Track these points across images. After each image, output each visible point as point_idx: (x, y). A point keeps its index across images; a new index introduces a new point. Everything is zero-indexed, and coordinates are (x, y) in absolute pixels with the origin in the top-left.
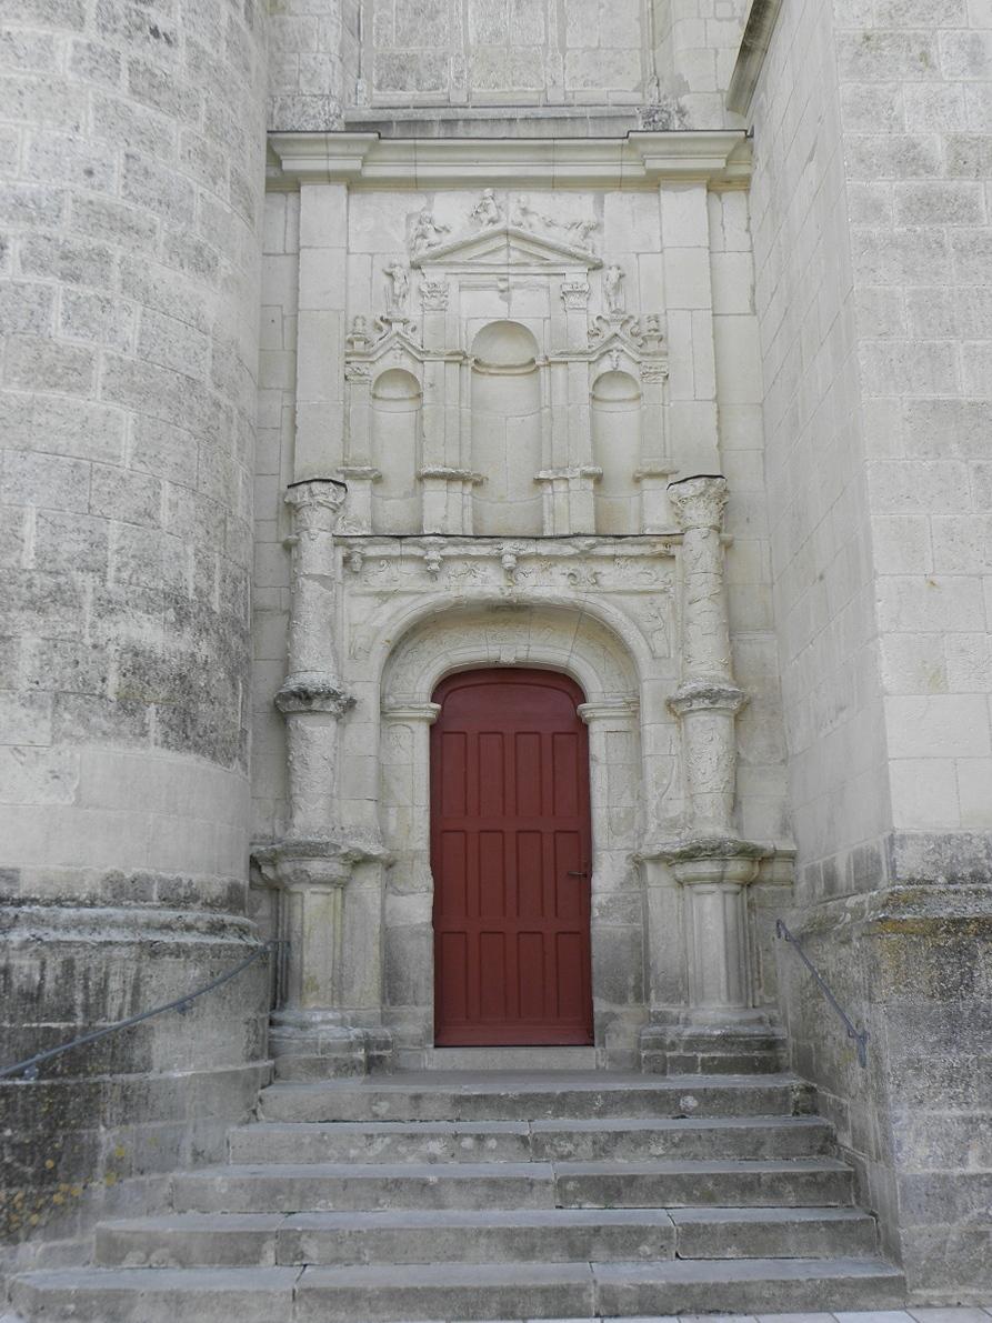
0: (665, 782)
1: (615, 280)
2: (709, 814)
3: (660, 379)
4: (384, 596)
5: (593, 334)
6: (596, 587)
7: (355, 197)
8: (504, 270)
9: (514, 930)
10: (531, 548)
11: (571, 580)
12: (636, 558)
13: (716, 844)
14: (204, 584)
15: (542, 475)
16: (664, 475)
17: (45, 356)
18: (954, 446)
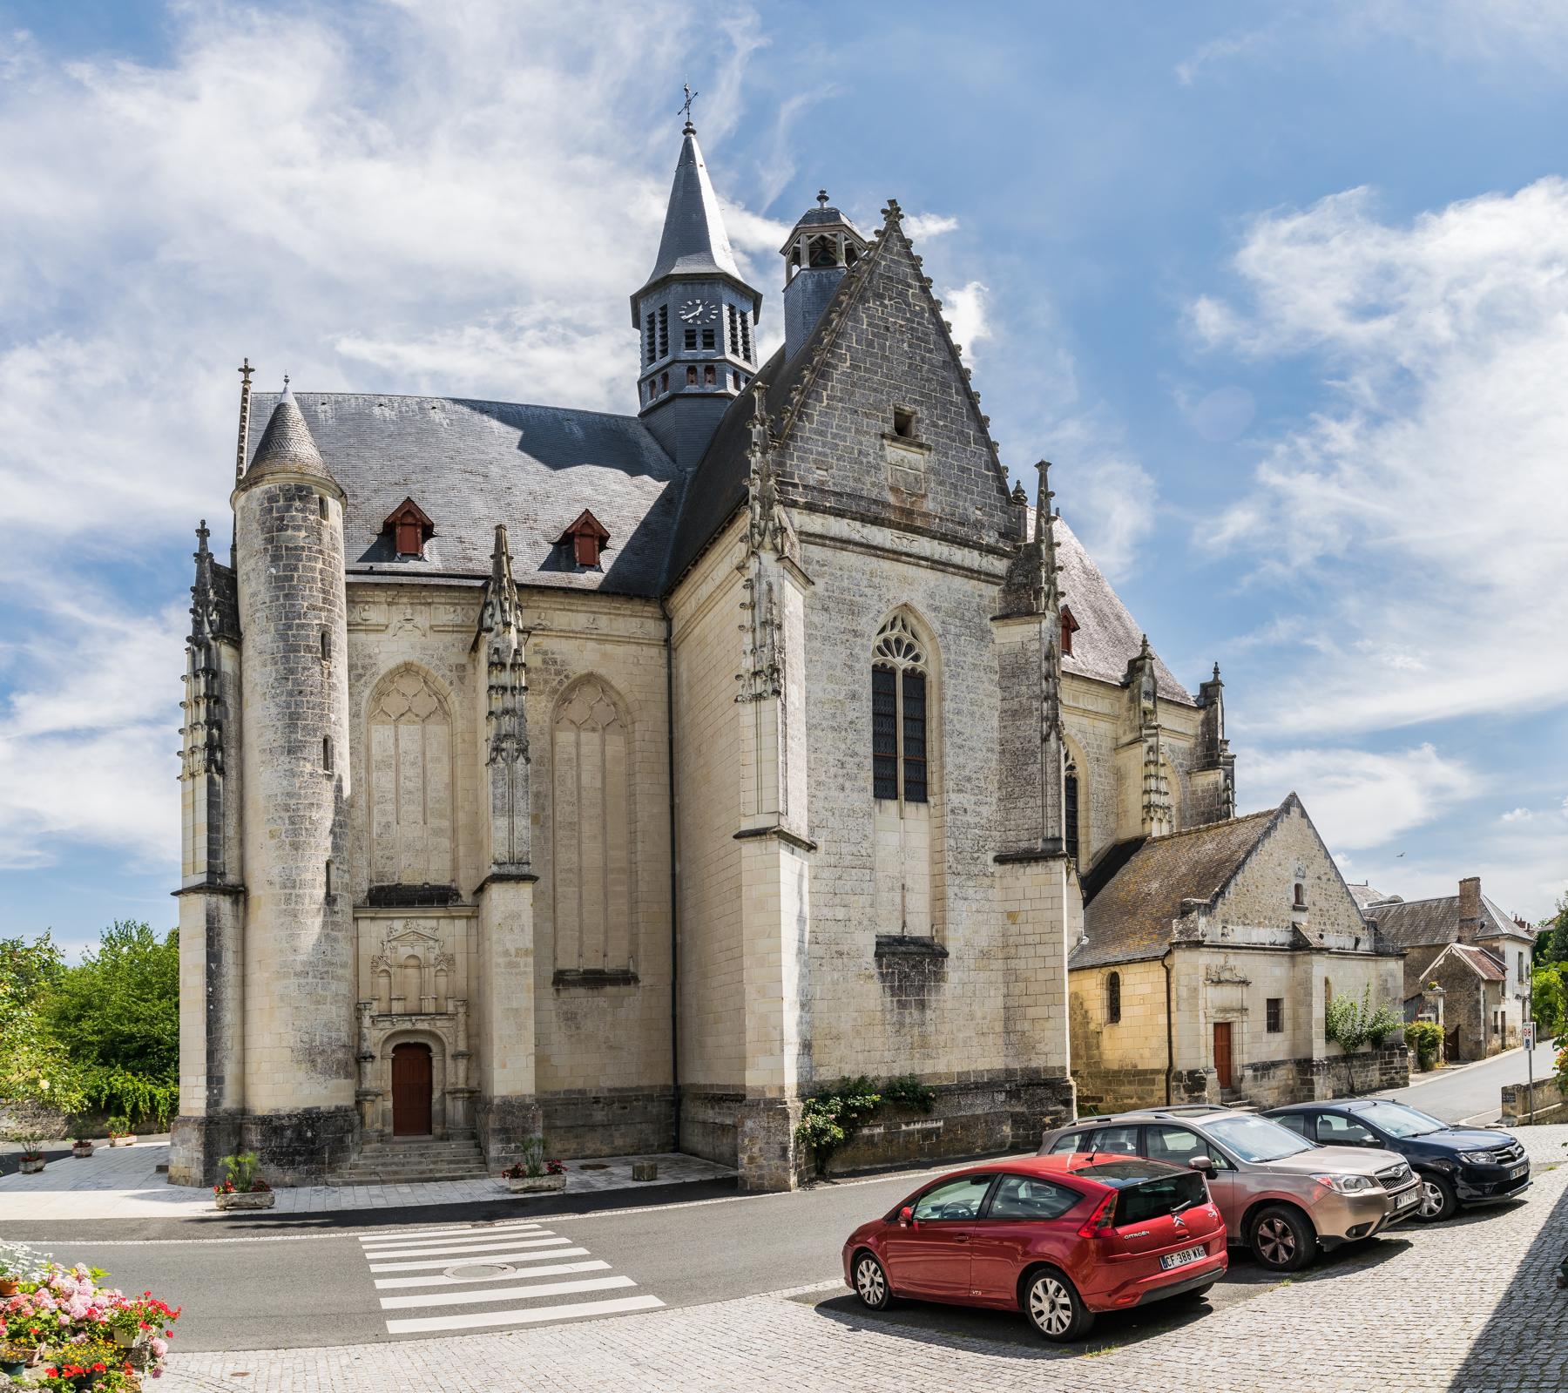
9: (414, 1109)
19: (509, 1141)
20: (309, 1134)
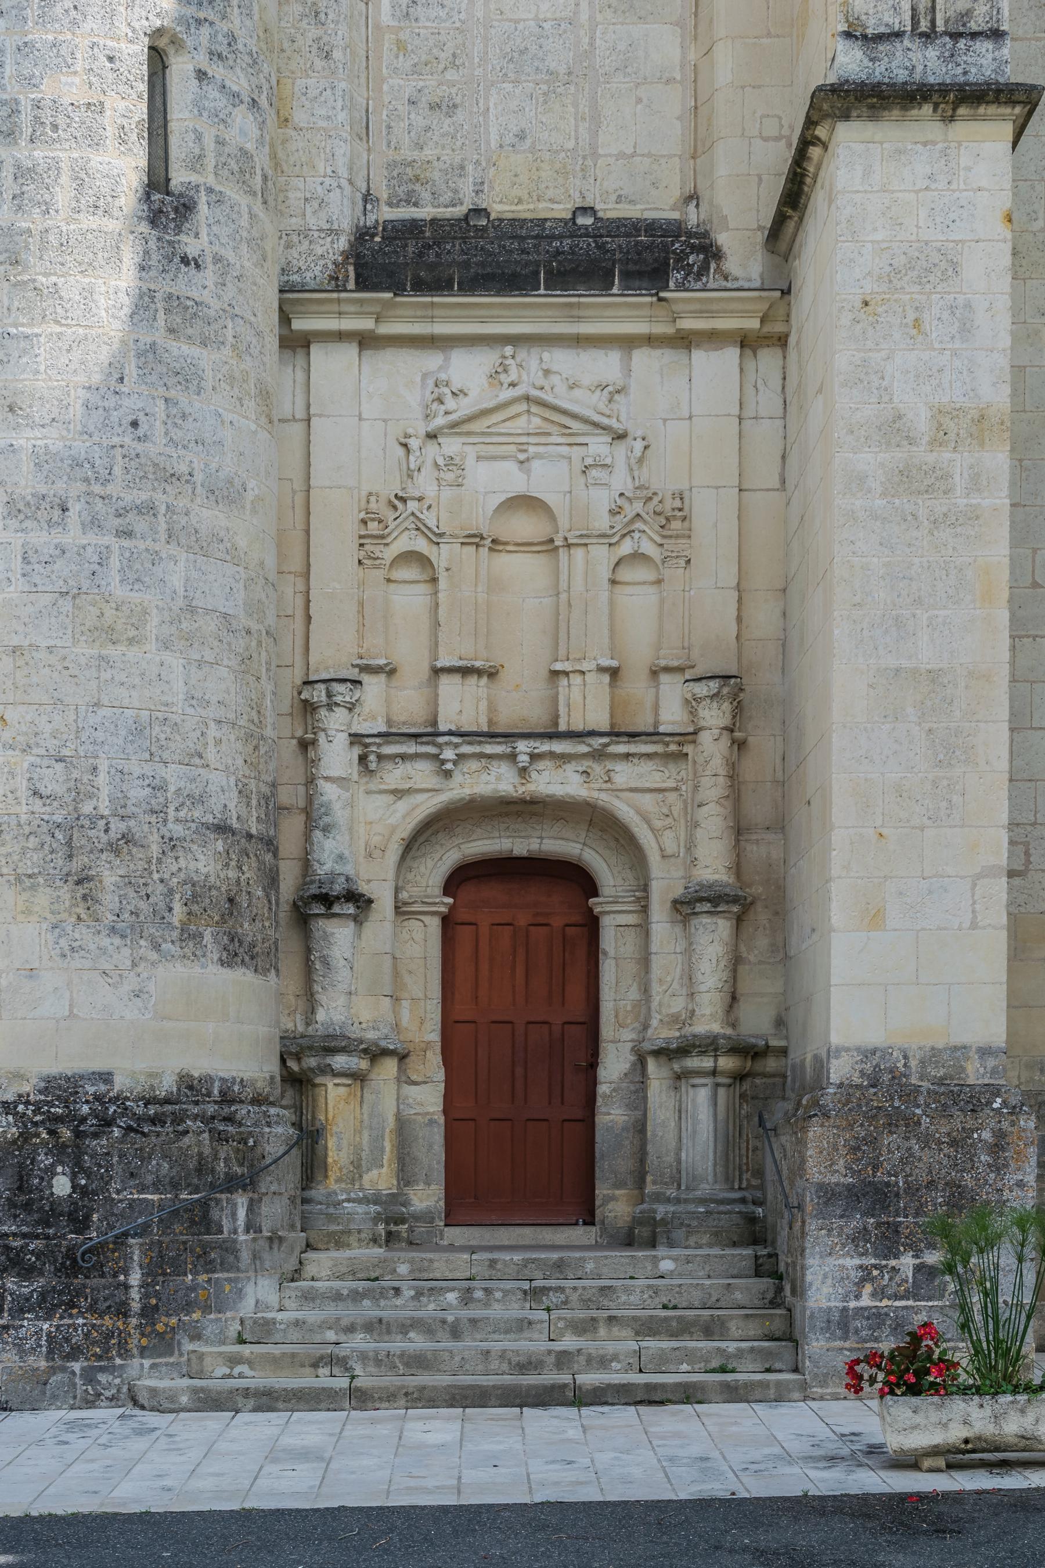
0: (669, 979)
1: (639, 454)
2: (708, 1012)
3: (682, 562)
4: (398, 793)
5: (613, 513)
6: (609, 785)
7: (367, 353)
8: (524, 439)
10: (545, 747)
11: (584, 777)
12: (649, 756)
13: (709, 1041)
14: (244, 814)
15: (558, 666)
16: (680, 670)
17: (107, 615)
18: (910, 710)
19: (889, 1241)
20: (62, 1186)
